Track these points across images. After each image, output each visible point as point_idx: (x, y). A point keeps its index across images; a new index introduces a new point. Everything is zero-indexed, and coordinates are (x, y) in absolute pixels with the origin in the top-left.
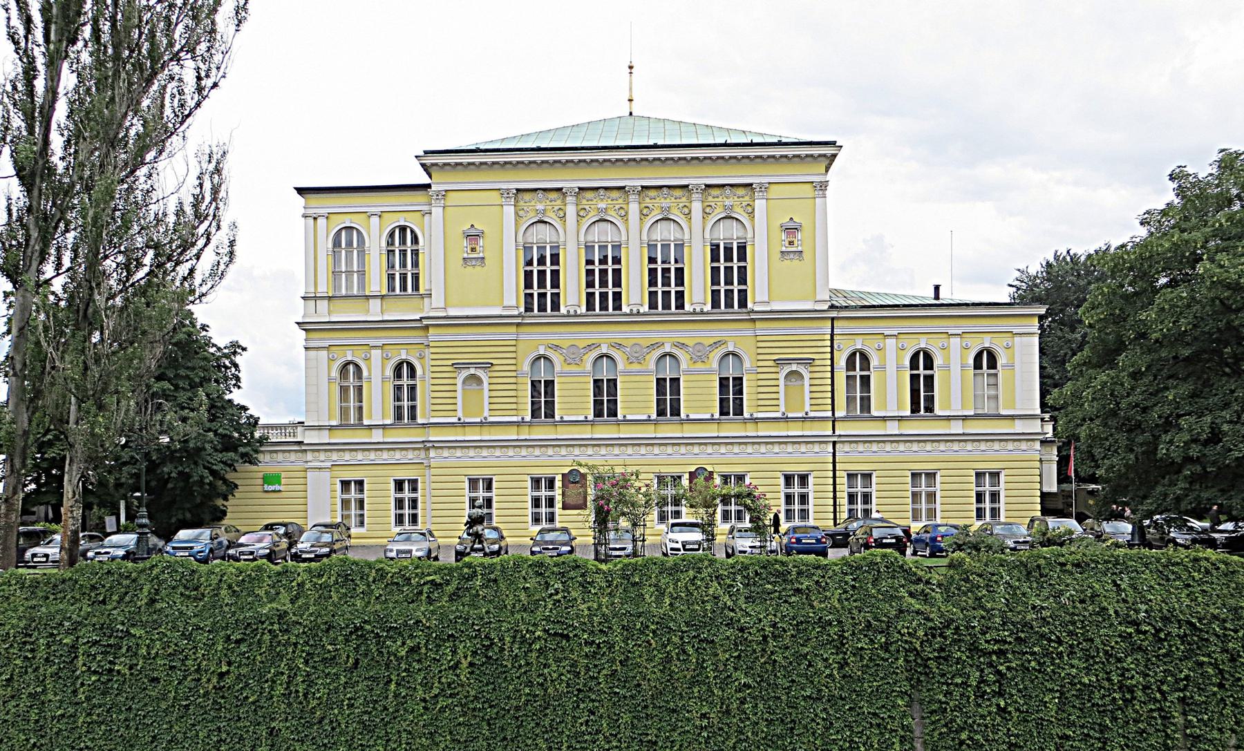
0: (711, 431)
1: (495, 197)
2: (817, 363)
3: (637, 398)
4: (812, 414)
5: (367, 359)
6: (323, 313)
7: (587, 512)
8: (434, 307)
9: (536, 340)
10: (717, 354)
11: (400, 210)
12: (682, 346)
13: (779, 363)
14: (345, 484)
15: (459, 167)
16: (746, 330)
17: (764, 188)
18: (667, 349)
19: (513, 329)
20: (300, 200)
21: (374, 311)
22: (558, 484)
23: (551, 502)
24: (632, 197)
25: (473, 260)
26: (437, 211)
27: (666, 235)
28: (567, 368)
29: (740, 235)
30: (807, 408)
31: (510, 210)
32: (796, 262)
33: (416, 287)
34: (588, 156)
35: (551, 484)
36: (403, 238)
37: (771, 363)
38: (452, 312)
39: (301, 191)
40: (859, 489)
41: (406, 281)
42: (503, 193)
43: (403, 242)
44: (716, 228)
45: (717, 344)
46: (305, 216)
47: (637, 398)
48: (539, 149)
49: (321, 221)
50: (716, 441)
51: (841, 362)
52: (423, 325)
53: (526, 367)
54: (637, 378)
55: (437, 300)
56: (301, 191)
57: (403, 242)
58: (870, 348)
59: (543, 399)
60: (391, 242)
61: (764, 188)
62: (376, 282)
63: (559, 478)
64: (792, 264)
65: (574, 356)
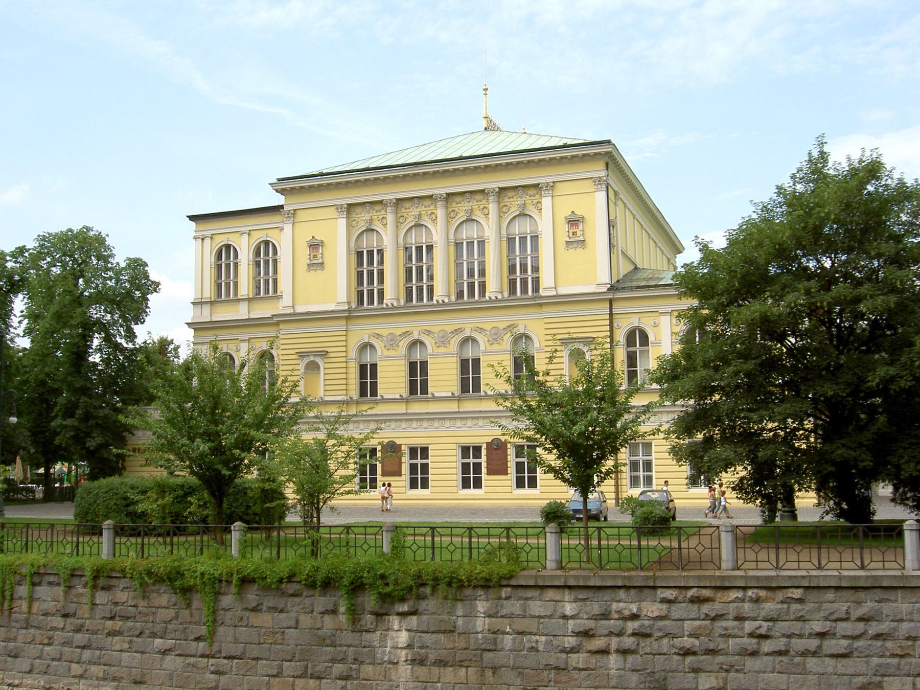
0: (400, 408)
1: (332, 212)
2: (332, 355)
3: (443, 377)
4: (327, 399)
5: (656, 325)
6: (206, 315)
7: (509, 477)
8: (282, 306)
9: (361, 332)
10: (404, 343)
11: (262, 229)
12: (378, 336)
13: (302, 355)
14: (465, 451)
15: (520, 166)
16: (533, 313)
17: (551, 186)
18: (468, 333)
19: (343, 322)
20: (193, 224)
21: (241, 312)
22: (484, 452)
23: (477, 467)
24: (491, 199)
25: (316, 265)
26: (288, 228)
27: (470, 234)
28: (386, 353)
29: (533, 229)
30: (322, 394)
31: (342, 223)
32: (579, 250)
33: (275, 291)
34: (568, 153)
35: (477, 449)
36: (265, 251)
37: (296, 357)
38: (562, 291)
39: (192, 218)
40: (641, 458)
41: (266, 287)
42: (338, 208)
43: (228, 257)
44: (409, 235)
45: (457, 331)
46: (196, 238)
47: (443, 377)
48: (368, 169)
49: (207, 241)
50: (408, 418)
51: (620, 336)
52: (276, 321)
53: (353, 353)
54: (444, 360)
55: (286, 301)
56: (192, 218)
57: (228, 257)
58: (646, 324)
59: (368, 378)
60: (257, 253)
61: (551, 186)
62: (245, 288)
63: (484, 446)
64: (576, 254)
65: (392, 343)
